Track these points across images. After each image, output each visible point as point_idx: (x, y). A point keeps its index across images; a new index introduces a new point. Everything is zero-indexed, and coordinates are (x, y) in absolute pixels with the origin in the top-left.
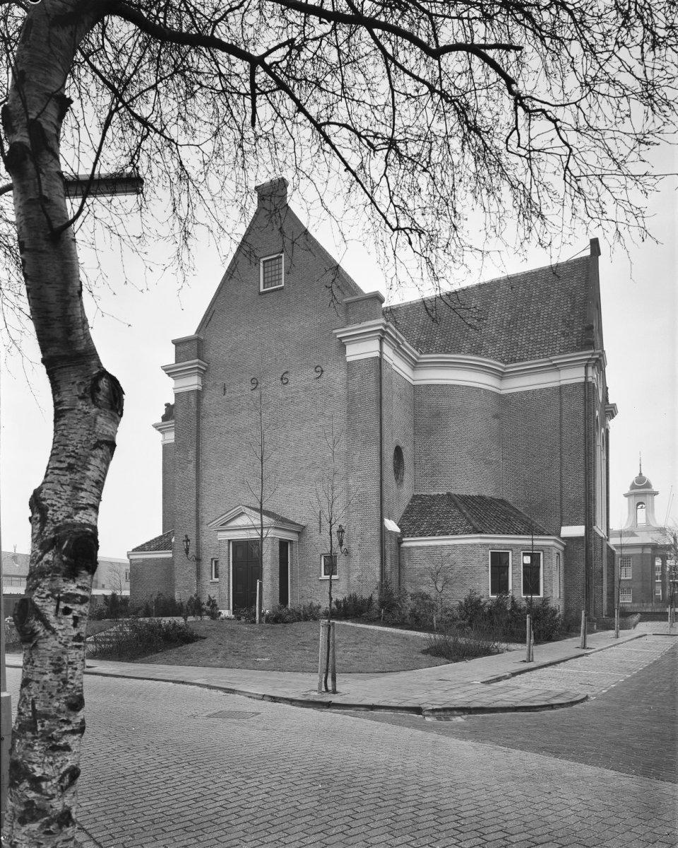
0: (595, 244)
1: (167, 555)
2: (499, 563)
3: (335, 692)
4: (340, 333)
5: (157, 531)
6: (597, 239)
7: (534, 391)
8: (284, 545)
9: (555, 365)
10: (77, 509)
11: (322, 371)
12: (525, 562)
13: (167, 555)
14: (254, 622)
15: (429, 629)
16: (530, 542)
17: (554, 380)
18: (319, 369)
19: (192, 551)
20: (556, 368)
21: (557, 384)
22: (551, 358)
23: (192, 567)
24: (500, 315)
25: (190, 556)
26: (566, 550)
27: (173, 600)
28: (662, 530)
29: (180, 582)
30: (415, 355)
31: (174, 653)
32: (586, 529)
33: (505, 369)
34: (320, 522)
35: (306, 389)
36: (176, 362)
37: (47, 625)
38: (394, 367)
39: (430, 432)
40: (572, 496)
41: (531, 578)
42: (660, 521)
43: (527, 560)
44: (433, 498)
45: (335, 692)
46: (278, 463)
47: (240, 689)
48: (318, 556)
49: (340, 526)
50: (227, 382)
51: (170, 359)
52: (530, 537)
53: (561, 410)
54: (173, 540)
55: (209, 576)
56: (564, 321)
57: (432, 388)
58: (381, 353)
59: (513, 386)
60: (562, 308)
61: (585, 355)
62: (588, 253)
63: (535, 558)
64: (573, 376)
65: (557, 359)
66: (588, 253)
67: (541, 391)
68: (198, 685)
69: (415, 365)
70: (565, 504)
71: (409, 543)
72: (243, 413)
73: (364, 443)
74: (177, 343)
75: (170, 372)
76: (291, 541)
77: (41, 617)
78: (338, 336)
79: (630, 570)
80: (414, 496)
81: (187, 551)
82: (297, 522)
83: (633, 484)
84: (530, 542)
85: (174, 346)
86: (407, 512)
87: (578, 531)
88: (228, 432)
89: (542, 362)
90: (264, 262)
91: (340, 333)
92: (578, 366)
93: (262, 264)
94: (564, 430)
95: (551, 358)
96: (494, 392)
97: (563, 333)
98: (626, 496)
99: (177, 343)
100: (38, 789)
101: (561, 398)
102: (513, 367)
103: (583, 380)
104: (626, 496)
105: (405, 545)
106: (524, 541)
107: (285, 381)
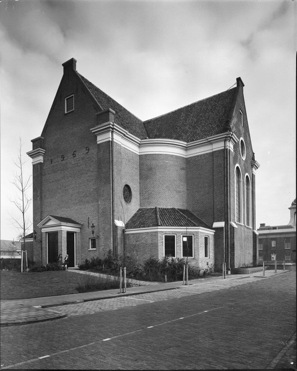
0: (239, 80)
2: (170, 241)
4: (93, 130)
6: (240, 78)
8: (70, 235)
11: (89, 149)
12: (184, 240)
16: (185, 230)
17: (209, 149)
18: (87, 149)
20: (210, 143)
22: (207, 138)
24: (192, 120)
30: (139, 141)
33: (140, 142)
34: (88, 223)
35: (83, 159)
36: (33, 149)
39: (147, 177)
40: (218, 207)
41: (188, 249)
43: (185, 239)
46: (72, 195)
48: (88, 239)
49: (93, 224)
50: (53, 158)
51: (30, 148)
52: (185, 227)
53: (213, 164)
56: (219, 120)
58: (112, 139)
60: (222, 113)
61: (223, 135)
62: (236, 86)
63: (190, 238)
64: (218, 146)
65: (210, 138)
66: (236, 86)
69: (140, 145)
70: (215, 211)
71: (130, 231)
72: (59, 172)
73: (105, 183)
74: (33, 141)
75: (31, 155)
76: (76, 232)
79: (289, 244)
82: (79, 223)
83: (293, 203)
84: (185, 230)
85: (32, 143)
86: (133, 217)
87: (221, 224)
88: (53, 182)
91: (93, 130)
94: (215, 174)
95: (207, 138)
96: (181, 157)
97: (217, 126)
98: (289, 209)
99: (33, 141)
101: (213, 158)
102: (148, 140)
103: (223, 148)
104: (289, 209)
105: (127, 233)
106: (183, 229)
107: (74, 156)
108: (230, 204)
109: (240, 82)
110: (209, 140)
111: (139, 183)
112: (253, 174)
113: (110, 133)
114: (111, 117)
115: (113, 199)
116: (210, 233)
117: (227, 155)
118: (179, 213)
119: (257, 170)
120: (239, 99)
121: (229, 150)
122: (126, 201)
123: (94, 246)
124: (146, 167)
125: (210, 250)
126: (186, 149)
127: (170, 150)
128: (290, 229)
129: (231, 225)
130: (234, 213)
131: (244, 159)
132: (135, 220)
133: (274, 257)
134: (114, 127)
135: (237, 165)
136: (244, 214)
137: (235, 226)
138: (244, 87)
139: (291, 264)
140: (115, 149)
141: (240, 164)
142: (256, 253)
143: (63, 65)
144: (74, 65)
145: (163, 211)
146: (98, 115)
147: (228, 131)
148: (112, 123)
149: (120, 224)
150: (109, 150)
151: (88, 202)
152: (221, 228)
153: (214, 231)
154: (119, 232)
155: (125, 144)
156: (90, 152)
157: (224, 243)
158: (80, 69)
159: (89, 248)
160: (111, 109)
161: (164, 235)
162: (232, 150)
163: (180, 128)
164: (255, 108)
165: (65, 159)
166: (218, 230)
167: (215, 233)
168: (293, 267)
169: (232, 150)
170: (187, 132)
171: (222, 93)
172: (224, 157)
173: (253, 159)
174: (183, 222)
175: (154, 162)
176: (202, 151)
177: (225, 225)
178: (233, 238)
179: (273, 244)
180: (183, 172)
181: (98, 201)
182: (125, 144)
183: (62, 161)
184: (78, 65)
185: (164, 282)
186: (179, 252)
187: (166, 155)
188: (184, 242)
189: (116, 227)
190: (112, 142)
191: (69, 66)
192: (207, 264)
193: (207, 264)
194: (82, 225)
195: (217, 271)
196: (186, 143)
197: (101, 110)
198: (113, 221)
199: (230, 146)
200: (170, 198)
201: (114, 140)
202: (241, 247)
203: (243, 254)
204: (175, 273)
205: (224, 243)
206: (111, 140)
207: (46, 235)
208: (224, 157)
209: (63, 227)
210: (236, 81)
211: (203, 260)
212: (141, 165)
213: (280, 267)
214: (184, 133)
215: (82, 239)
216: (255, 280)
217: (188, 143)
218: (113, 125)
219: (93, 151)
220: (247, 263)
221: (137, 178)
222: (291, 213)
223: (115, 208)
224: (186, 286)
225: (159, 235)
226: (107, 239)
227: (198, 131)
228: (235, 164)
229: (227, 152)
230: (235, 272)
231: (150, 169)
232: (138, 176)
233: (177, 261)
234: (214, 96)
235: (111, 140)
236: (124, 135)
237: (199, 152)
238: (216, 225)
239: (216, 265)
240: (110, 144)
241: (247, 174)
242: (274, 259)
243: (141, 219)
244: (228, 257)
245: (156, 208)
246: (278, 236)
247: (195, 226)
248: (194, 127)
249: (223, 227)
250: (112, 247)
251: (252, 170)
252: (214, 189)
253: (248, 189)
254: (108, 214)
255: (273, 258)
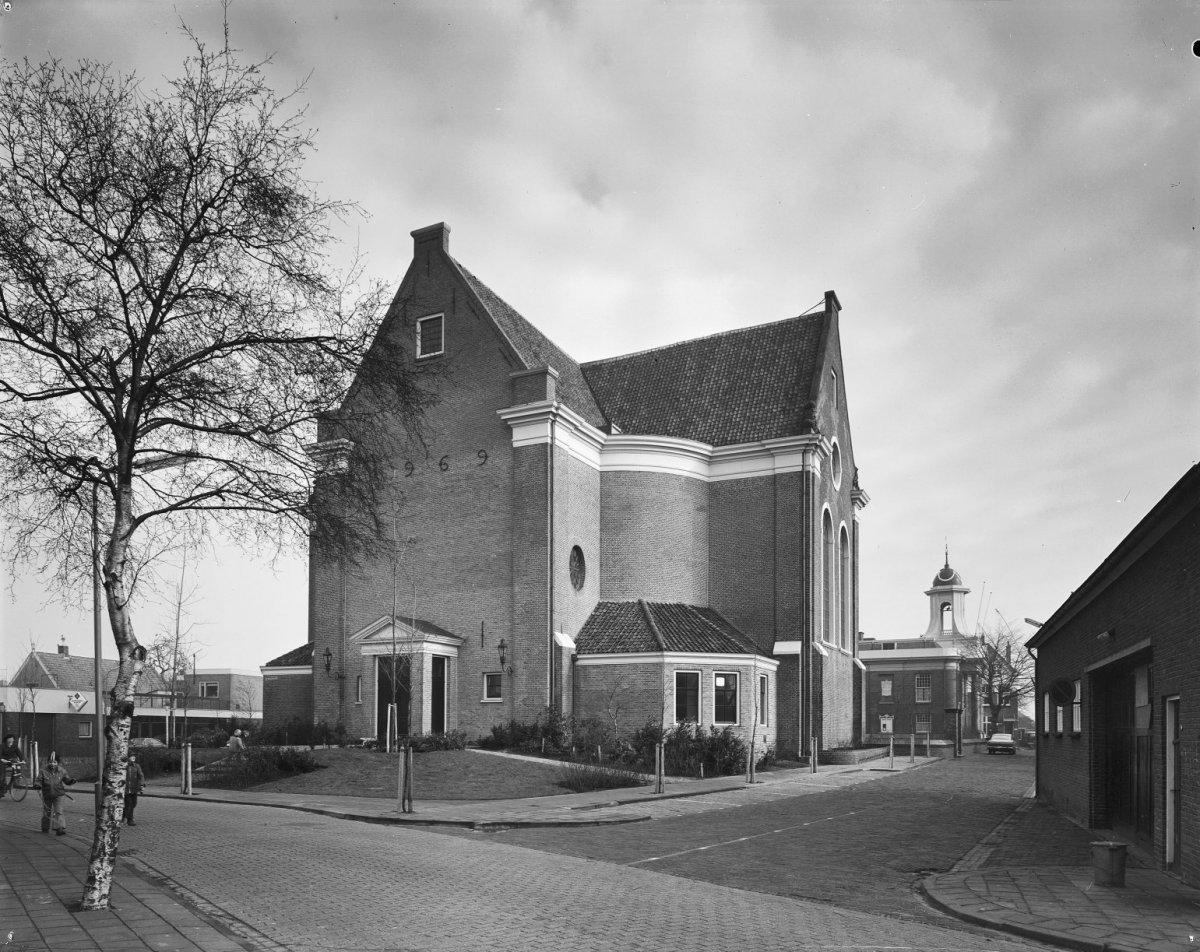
0: (830, 297)
1: (306, 671)
2: (687, 685)
3: (410, 812)
4: (505, 414)
5: (302, 640)
7: (746, 480)
8: (438, 662)
9: (769, 450)
10: (127, 696)
11: (486, 457)
12: (718, 685)
13: (306, 671)
14: (385, 751)
15: (564, 756)
17: (764, 467)
19: (334, 667)
20: (770, 453)
21: (770, 473)
22: (764, 442)
23: (334, 686)
24: (716, 382)
25: (332, 672)
26: (781, 674)
27: (310, 724)
28: (971, 641)
29: (321, 705)
30: (602, 438)
31: (287, 782)
32: (803, 646)
33: (606, 440)
35: (468, 477)
37: (115, 734)
38: (571, 452)
41: (726, 706)
42: (968, 629)
43: (721, 682)
44: (621, 606)
45: (410, 812)
47: (330, 810)
48: (479, 674)
54: (313, 654)
55: (354, 698)
56: (786, 395)
57: (622, 475)
59: (720, 473)
61: (800, 440)
62: (822, 308)
64: (788, 464)
65: (770, 443)
66: (822, 308)
67: (754, 480)
68: (296, 808)
69: (603, 448)
70: (778, 618)
71: (586, 660)
76: (448, 657)
77: (113, 732)
78: (503, 417)
79: (928, 693)
80: (600, 604)
81: (328, 667)
82: (456, 633)
86: (588, 623)
87: (793, 647)
89: (754, 446)
90: (422, 323)
91: (505, 414)
92: (796, 452)
93: (418, 325)
94: (779, 527)
97: (784, 410)
98: (928, 593)
100: (111, 785)
103: (800, 469)
104: (928, 593)
105: (579, 663)
107: (444, 467)
108: (813, 601)
109: (833, 302)
110: (767, 447)
111: (598, 541)
112: (854, 521)
113: (549, 425)
114: (551, 384)
115: (551, 583)
116: (769, 666)
117: (808, 485)
118: (697, 617)
119: (863, 509)
120: (830, 345)
121: (813, 474)
122: (575, 585)
123: (493, 692)
124: (618, 500)
125: (770, 707)
126: (710, 460)
127: (676, 462)
128: (927, 650)
129: (814, 650)
130: (820, 621)
131: (838, 486)
132: (595, 630)
133: (888, 723)
134: (560, 412)
135: (826, 505)
136: (837, 621)
137: (824, 652)
138: (840, 312)
139: (942, 743)
140: (558, 461)
141: (830, 501)
142: (861, 715)
143: (413, 234)
144: (445, 240)
145: (659, 609)
146: (515, 379)
147: (813, 432)
148: (555, 404)
149: (566, 641)
150: (546, 465)
151: (482, 586)
152: (793, 658)
153: (778, 663)
154: (566, 661)
155: (578, 448)
156: (488, 462)
157: (799, 685)
158: (457, 250)
159: (481, 697)
160: (551, 370)
161: (675, 672)
162: (818, 474)
163: (687, 400)
164: (858, 344)
165: (416, 471)
166: (785, 659)
167: (778, 666)
168: (948, 750)
169: (818, 474)
170: (707, 414)
171: (789, 322)
172: (801, 490)
173: (855, 484)
174: (714, 642)
175: (636, 492)
176: (752, 469)
177: (802, 650)
178: (819, 679)
179: (887, 689)
180: (703, 516)
181: (511, 584)
182: (578, 448)
183: (407, 476)
184: (452, 237)
185: (699, 777)
186: (707, 711)
187: (664, 474)
188: (718, 689)
189: (559, 649)
190: (552, 446)
191: (430, 242)
192: (765, 741)
193: (765, 741)
194: (465, 641)
195: (785, 755)
196: (710, 448)
197: (522, 367)
198: (552, 635)
199: (815, 463)
200: (677, 583)
201: (557, 442)
202: (831, 699)
203: (838, 722)
204: (719, 757)
205: (799, 685)
206: (549, 441)
207: (374, 661)
208: (801, 490)
209: (425, 645)
210: (824, 297)
211: (759, 731)
212: (605, 495)
213: (902, 750)
214: (699, 416)
215: (462, 672)
216: (873, 776)
217: (717, 449)
218: (557, 409)
219: (500, 462)
220: (842, 737)
221: (596, 527)
222: (932, 608)
223: (556, 605)
224: (752, 785)
225: (666, 671)
226: (535, 676)
227: (737, 417)
228: (822, 504)
229: (808, 479)
230: (827, 758)
231: (628, 507)
232: (598, 524)
233: (709, 734)
234: (769, 327)
235: (549, 441)
236: (576, 428)
237: (740, 470)
238: (782, 647)
239: (779, 741)
240: (544, 453)
241: (843, 523)
242: (890, 728)
243: (602, 631)
244: (808, 725)
245: (640, 603)
246: (898, 668)
247: (741, 651)
248: (725, 405)
249: (797, 655)
250: (549, 695)
251: (853, 511)
252: (772, 561)
253: (843, 558)
254: (542, 616)
255: (884, 726)
